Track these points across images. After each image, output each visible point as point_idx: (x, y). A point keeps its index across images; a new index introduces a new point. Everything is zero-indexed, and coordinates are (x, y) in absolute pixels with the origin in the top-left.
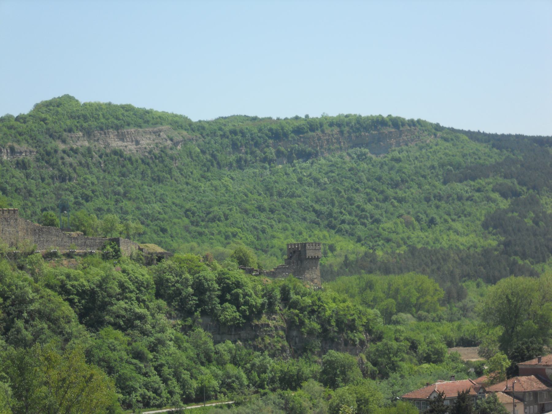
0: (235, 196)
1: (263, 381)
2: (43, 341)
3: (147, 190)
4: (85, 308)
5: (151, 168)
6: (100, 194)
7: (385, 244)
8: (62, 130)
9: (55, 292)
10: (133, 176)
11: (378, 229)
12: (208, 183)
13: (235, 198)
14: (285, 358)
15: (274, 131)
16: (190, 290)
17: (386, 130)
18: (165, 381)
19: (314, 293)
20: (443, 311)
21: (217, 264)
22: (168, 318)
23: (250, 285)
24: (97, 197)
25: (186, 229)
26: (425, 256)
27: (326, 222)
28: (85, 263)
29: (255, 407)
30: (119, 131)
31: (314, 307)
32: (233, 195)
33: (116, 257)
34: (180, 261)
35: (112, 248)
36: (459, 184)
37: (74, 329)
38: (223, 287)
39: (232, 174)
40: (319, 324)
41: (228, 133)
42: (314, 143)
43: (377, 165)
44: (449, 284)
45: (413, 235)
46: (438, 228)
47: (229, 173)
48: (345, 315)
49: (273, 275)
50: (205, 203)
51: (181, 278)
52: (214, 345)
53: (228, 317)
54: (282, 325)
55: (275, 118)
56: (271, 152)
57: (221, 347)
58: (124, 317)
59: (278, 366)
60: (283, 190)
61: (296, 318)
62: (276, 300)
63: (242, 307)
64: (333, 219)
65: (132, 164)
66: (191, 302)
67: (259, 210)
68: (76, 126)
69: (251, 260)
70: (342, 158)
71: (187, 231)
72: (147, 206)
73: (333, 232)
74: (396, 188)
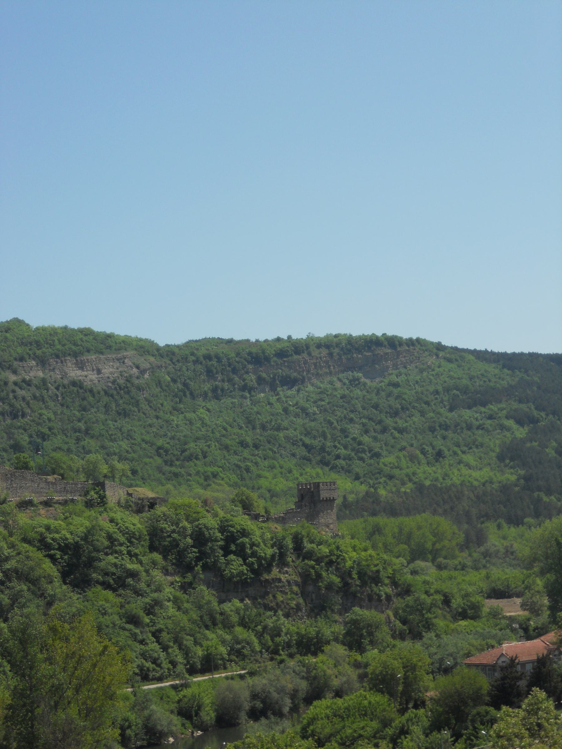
0: (212, 430)
1: (277, 645)
2: (23, 606)
3: (112, 426)
4: (68, 565)
5: (116, 401)
6: (58, 432)
7: (388, 481)
8: (12, 358)
9: (34, 547)
10: (95, 410)
11: (378, 464)
12: (181, 416)
13: (213, 433)
14: (301, 619)
15: (254, 355)
16: (189, 540)
17: (381, 351)
18: (165, 648)
19: (331, 541)
20: (463, 557)
21: (219, 510)
22: (165, 575)
23: (258, 533)
24: (55, 435)
25: (159, 469)
26: (436, 495)
27: (319, 458)
28: (66, 512)
29: (272, 677)
30: (78, 359)
31: (332, 557)
32: (210, 429)
33: (102, 504)
34: (176, 507)
35: (97, 493)
36: (467, 411)
37: (57, 591)
38: (227, 536)
39: (209, 405)
40: (338, 577)
41: (202, 359)
42: (300, 367)
43: (373, 391)
44: (466, 526)
45: (418, 471)
46: (447, 462)
47: (204, 404)
48: (368, 566)
49: (282, 520)
50: (179, 440)
51: (177, 527)
52: (219, 605)
53: (235, 571)
54: (296, 579)
55: (253, 340)
56: (251, 379)
57: (227, 607)
58: (114, 574)
59: (294, 628)
60: (267, 422)
61: (312, 571)
62: (288, 551)
63: (250, 559)
64: (326, 454)
65: (94, 396)
66: (190, 555)
67: (242, 446)
68: (28, 353)
69: (255, 504)
70: (332, 384)
71: (160, 472)
72: (112, 444)
73: (327, 469)
74: (395, 417)
